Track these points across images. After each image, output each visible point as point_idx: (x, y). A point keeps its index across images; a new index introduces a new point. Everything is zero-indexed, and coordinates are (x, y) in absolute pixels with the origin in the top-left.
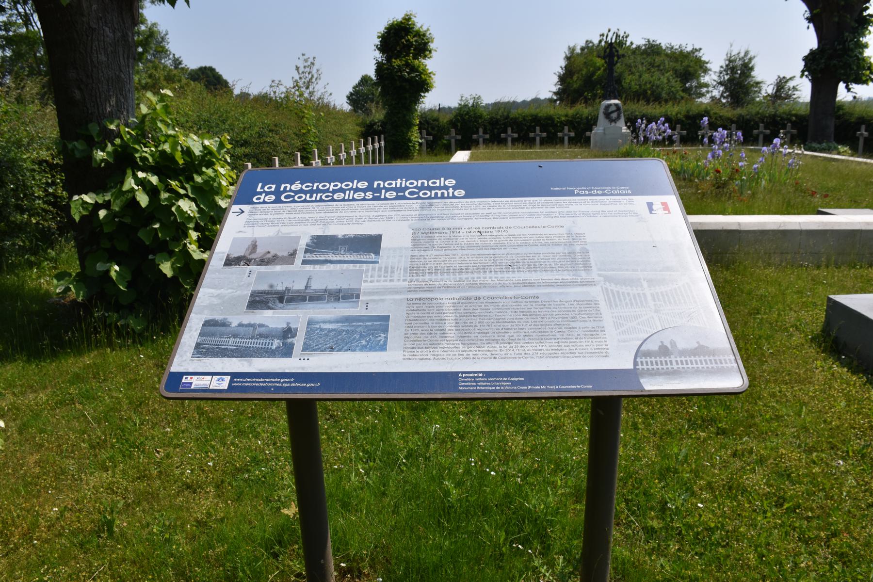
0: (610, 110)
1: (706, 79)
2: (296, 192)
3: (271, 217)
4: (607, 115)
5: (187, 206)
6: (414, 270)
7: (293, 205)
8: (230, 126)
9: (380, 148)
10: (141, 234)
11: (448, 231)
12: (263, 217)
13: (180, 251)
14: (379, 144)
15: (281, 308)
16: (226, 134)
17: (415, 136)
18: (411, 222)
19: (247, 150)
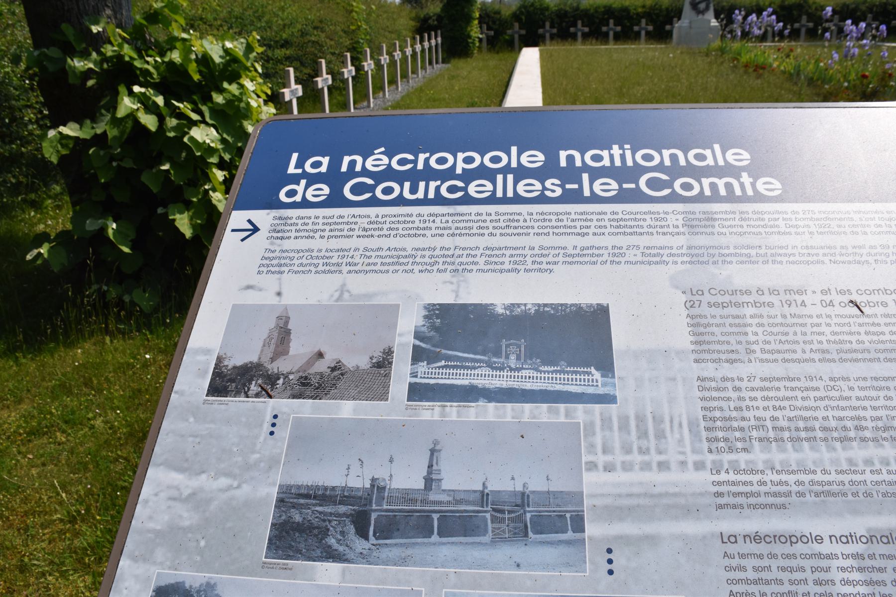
2: (379, 177)
3: (323, 244)
5: (204, 135)
6: (720, 430)
7: (372, 211)
8: (267, 22)
9: (436, 46)
10: (145, 178)
11: (774, 299)
12: (303, 244)
13: (199, 200)
14: (436, 41)
15: (365, 558)
16: (254, 33)
17: (475, 32)
18: (672, 269)
19: (288, 52)
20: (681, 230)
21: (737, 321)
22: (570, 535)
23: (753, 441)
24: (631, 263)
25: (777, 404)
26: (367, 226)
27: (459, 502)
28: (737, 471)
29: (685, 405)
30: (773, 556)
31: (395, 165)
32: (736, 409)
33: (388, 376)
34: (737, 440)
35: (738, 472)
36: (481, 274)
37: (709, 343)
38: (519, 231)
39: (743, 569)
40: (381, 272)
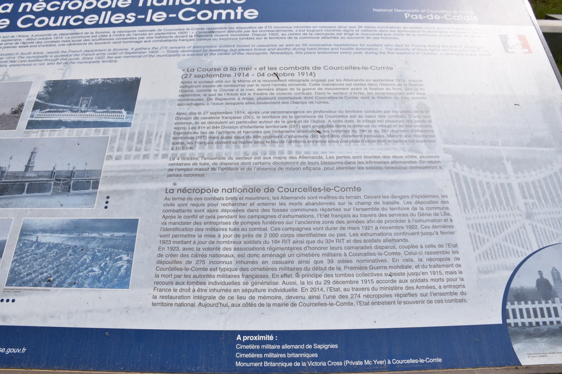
6: (180, 139)
11: (232, 73)
18: (181, 58)
20: (193, 38)
21: (207, 84)
22: (91, 190)
23: (197, 144)
24: (160, 56)
25: (215, 125)
26: (25, 41)
27: (39, 177)
28: (184, 159)
29: (167, 126)
30: (190, 199)
31: (49, 8)
32: (192, 128)
33: (18, 117)
34: (188, 143)
35: (184, 159)
36: (80, 64)
37: (189, 95)
38: (106, 41)
39: (173, 205)
40: (27, 65)
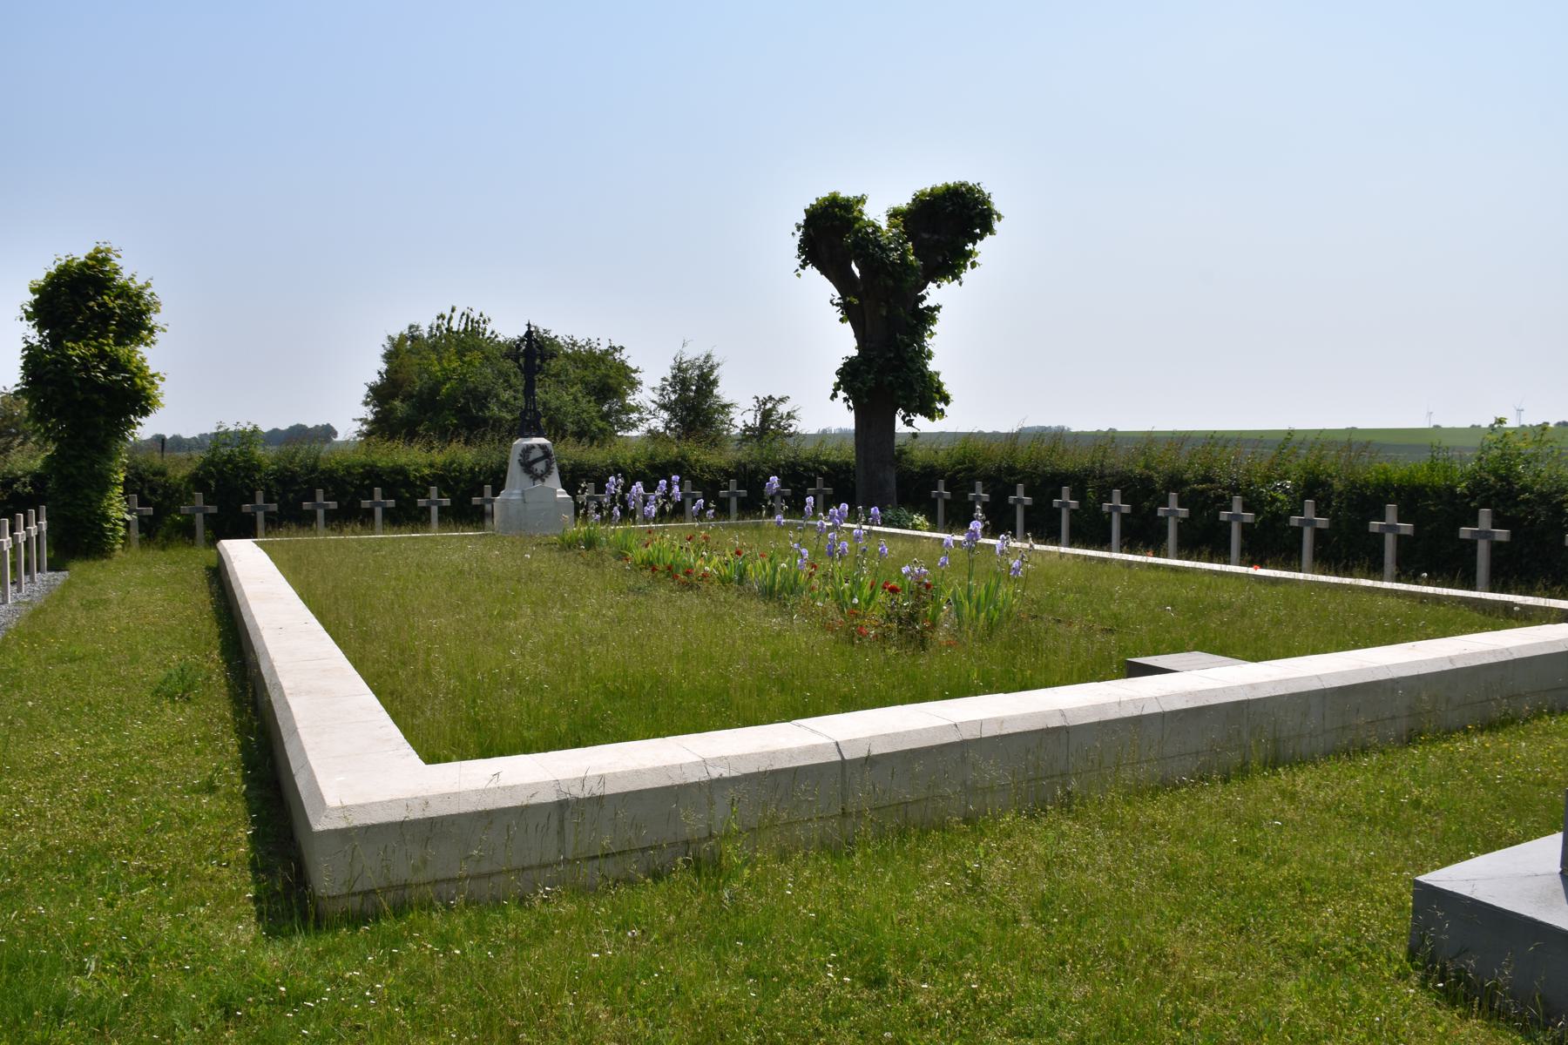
0: (532, 457)
1: (633, 399)
4: (527, 466)
14: (36, 526)
17: (118, 509)
